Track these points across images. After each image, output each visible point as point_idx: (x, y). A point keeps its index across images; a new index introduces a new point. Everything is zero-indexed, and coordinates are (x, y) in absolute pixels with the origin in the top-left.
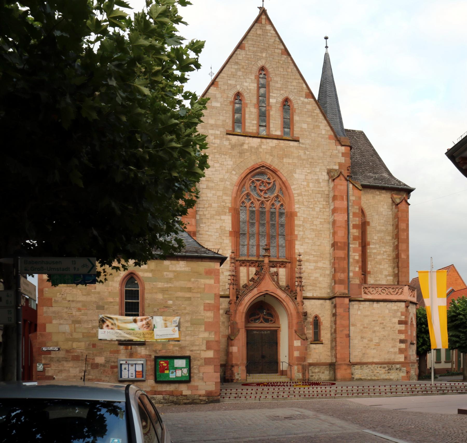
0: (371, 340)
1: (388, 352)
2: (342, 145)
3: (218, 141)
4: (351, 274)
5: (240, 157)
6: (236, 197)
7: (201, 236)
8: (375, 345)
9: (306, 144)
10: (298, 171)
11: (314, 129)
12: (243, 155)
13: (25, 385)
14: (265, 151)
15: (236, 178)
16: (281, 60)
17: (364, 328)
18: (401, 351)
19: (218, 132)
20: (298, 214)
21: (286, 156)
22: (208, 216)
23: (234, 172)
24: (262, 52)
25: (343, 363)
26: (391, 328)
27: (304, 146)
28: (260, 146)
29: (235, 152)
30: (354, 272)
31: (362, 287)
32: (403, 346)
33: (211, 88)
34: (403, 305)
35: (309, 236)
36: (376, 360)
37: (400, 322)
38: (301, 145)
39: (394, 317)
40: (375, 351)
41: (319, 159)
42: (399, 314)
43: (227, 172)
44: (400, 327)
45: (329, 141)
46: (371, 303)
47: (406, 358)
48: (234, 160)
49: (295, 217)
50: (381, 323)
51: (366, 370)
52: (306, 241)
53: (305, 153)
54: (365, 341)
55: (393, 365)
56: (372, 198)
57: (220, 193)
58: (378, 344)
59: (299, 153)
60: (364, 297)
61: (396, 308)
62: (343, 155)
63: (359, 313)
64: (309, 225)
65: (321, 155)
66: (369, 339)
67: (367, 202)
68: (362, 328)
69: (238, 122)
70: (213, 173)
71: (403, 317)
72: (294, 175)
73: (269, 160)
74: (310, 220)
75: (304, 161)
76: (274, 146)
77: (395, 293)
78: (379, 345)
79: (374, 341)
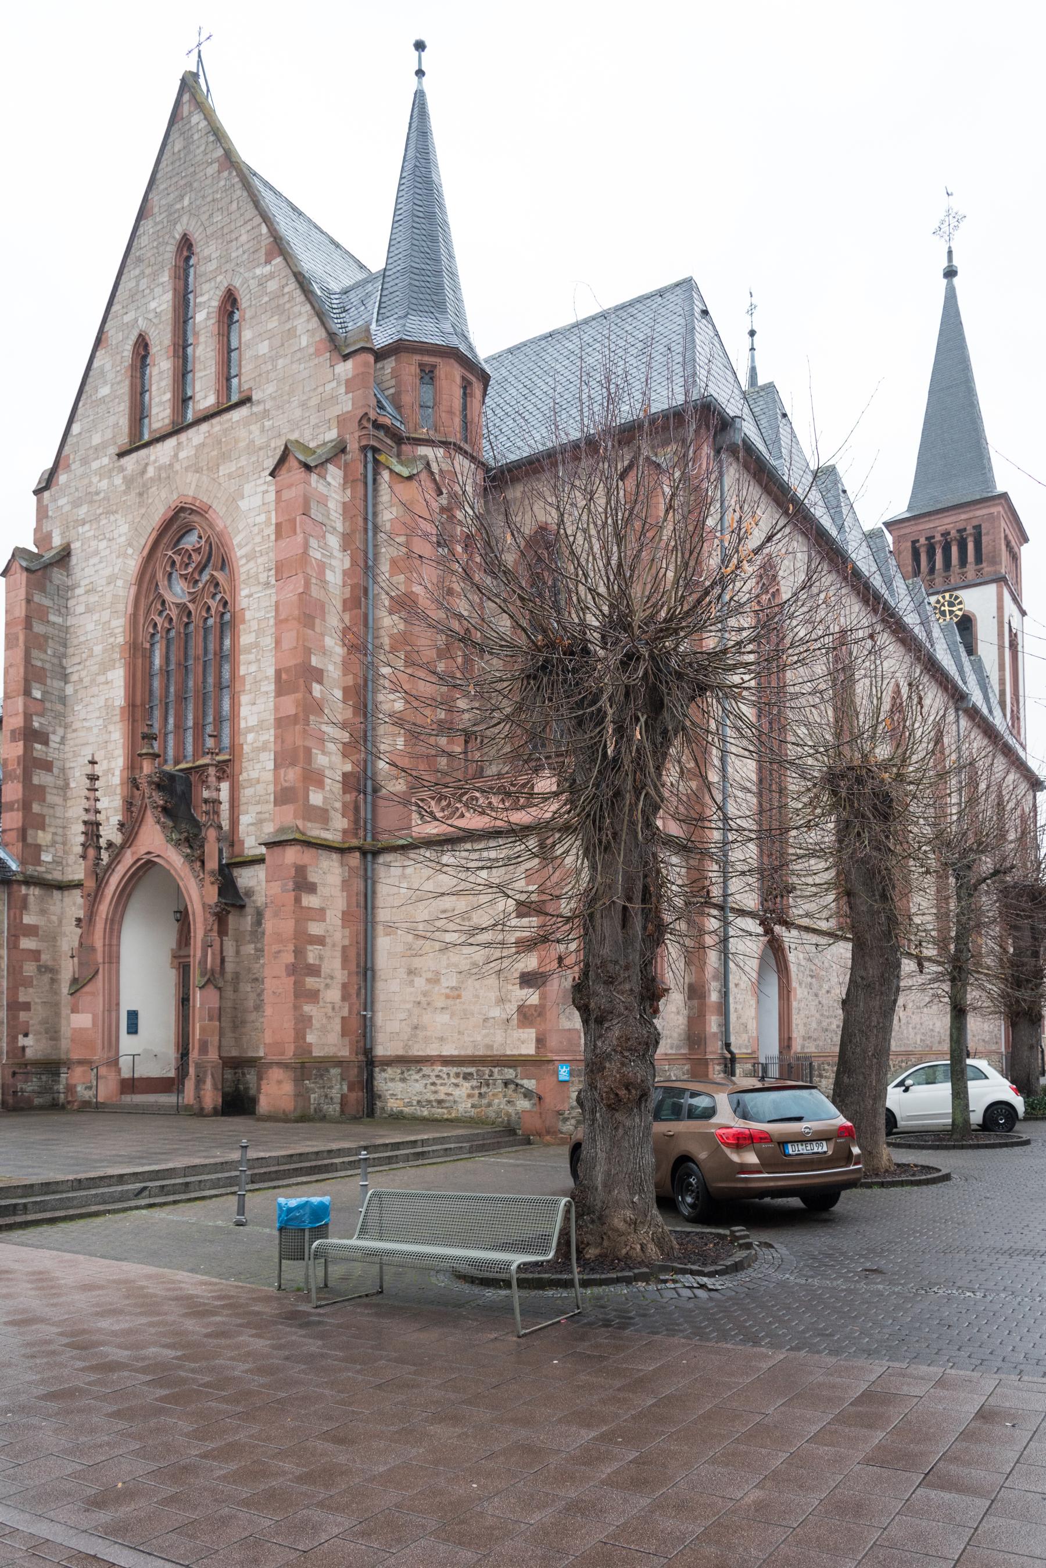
0: (435, 980)
1: (486, 1020)
2: (346, 357)
3: (104, 484)
5: (141, 505)
6: (135, 615)
7: (74, 735)
8: (448, 997)
9: (264, 401)
10: (248, 488)
11: (283, 345)
12: (145, 496)
13: (723, 1152)
15: (133, 564)
16: (217, 192)
18: (526, 1016)
19: (105, 461)
20: (248, 615)
21: (225, 457)
22: (87, 681)
23: (130, 551)
24: (182, 197)
28: (176, 455)
29: (132, 498)
32: (532, 997)
33: (98, 354)
36: (449, 1050)
40: (444, 1018)
41: (293, 431)
43: (118, 557)
45: (316, 361)
47: (540, 1041)
48: (130, 517)
49: (241, 627)
51: (417, 1085)
52: (263, 689)
53: (263, 430)
54: (420, 982)
55: (496, 1070)
58: (455, 994)
59: (250, 433)
65: (298, 413)
66: (430, 975)
69: (139, 413)
70: (96, 568)
72: (239, 503)
73: (189, 487)
75: (261, 453)
76: (202, 441)
78: (459, 997)
79: (445, 982)
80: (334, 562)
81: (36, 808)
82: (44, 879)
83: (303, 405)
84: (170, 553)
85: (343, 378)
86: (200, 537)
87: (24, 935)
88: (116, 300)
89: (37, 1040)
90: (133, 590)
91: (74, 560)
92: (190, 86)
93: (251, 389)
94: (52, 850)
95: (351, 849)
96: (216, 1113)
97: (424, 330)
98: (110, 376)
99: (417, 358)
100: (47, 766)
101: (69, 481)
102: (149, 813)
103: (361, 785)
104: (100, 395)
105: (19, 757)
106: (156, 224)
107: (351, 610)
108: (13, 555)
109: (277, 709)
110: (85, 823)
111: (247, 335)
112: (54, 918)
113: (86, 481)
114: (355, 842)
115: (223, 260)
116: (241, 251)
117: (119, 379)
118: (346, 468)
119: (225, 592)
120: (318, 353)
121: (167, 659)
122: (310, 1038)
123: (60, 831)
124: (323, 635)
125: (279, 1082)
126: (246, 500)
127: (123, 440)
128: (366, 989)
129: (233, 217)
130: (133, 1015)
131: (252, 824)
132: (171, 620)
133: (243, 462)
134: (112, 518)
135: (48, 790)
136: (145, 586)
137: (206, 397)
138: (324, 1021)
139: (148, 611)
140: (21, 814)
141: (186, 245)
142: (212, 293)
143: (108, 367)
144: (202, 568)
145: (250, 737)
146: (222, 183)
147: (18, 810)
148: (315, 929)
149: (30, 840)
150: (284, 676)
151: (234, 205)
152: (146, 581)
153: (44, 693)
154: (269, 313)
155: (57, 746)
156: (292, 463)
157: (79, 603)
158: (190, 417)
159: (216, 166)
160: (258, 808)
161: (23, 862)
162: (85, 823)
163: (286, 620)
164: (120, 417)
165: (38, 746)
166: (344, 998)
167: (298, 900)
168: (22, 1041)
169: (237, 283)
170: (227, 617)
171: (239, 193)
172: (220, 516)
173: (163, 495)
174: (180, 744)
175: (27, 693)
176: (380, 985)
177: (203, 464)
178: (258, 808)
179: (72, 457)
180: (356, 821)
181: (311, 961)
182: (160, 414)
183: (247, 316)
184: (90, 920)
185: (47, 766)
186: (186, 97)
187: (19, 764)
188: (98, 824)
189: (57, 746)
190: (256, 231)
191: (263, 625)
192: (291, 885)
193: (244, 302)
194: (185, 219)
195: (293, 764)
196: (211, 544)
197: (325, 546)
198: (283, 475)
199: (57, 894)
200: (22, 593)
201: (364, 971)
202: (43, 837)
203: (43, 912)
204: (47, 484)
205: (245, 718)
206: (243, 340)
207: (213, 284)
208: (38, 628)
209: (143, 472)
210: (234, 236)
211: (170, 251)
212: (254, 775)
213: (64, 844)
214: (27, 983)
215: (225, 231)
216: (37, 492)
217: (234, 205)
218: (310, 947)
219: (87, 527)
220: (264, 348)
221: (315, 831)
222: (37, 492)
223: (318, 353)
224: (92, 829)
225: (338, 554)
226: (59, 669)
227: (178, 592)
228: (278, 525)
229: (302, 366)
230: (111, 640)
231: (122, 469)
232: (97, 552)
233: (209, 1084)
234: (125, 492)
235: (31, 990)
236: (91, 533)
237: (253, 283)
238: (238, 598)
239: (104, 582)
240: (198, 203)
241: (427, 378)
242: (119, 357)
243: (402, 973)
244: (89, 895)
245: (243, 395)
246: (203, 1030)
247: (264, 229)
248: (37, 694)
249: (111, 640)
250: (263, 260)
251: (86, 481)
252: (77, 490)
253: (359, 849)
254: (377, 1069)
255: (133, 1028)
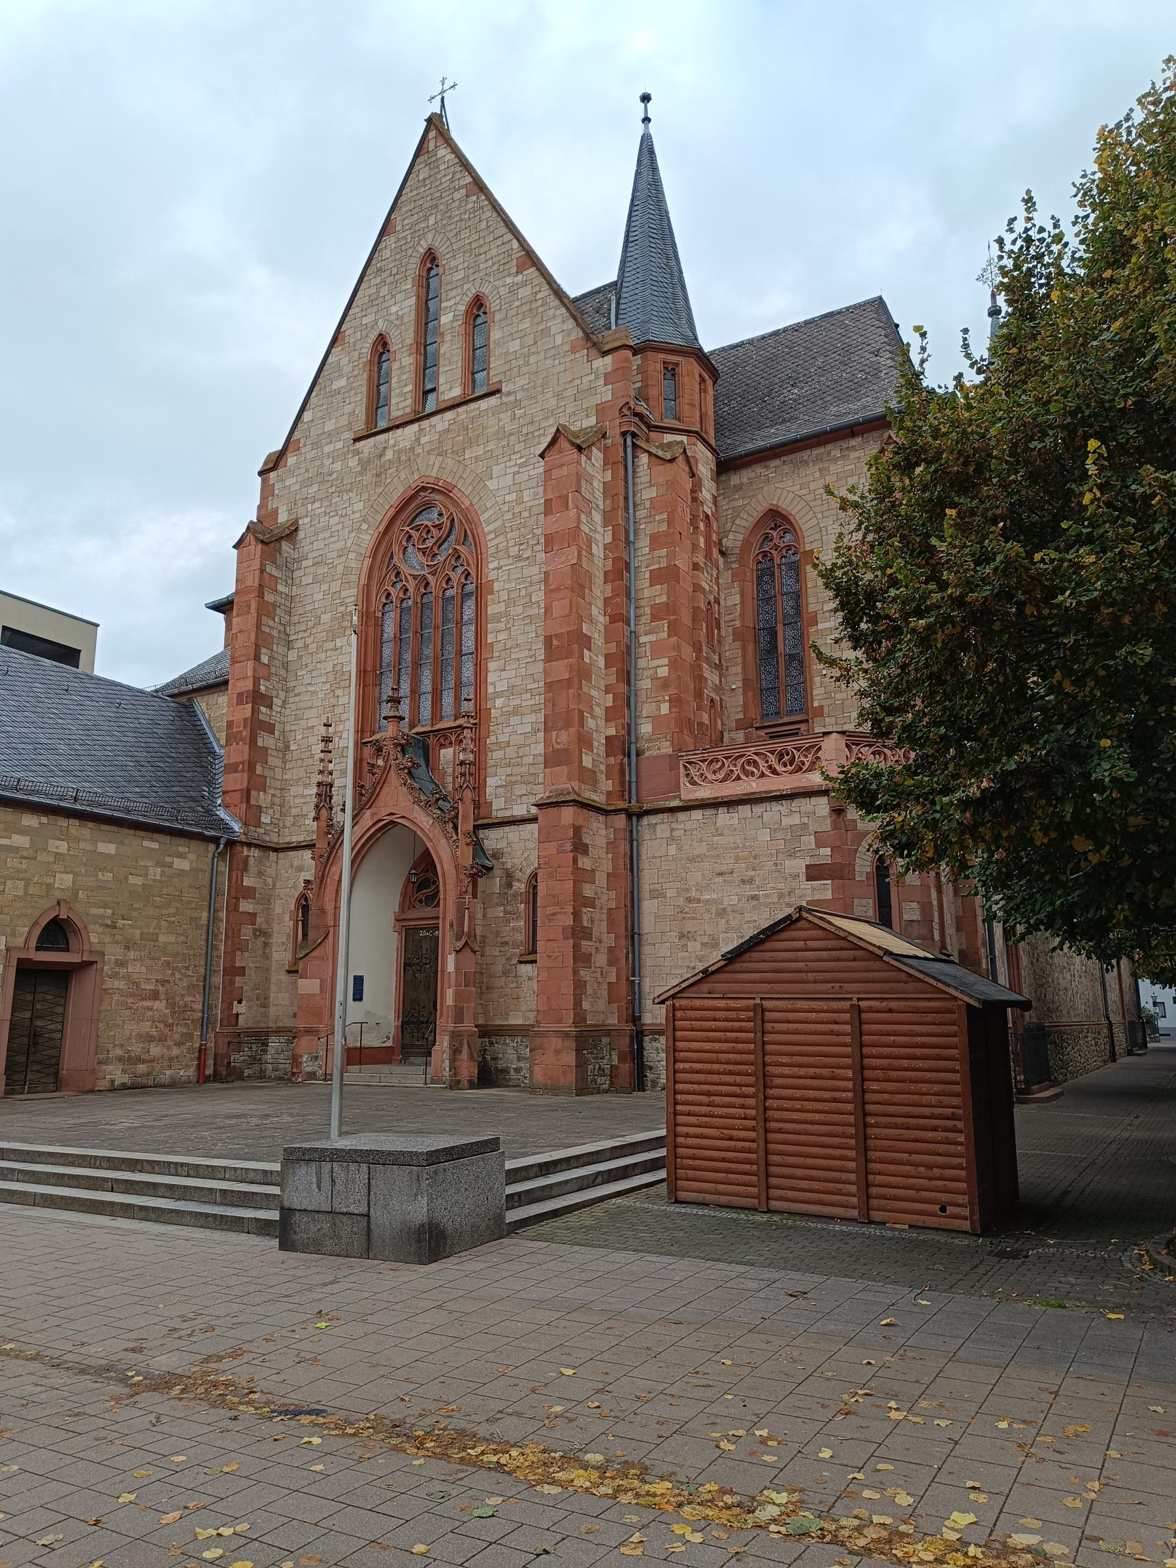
2: (605, 353)
4: (646, 728)
6: (368, 585)
11: (535, 343)
14: (419, 452)
15: (368, 539)
17: (689, 900)
20: (497, 586)
21: (471, 442)
22: (312, 648)
24: (426, 218)
25: (553, 1027)
26: (781, 896)
27: (512, 398)
28: (418, 440)
29: (369, 477)
30: (655, 720)
31: (681, 763)
34: (822, 806)
35: (521, 639)
37: (814, 873)
38: (505, 399)
39: (792, 855)
42: (809, 841)
44: (813, 889)
46: (709, 812)
50: (743, 881)
53: (514, 418)
56: (817, 475)
57: (335, 586)
59: (500, 420)
60: (689, 793)
61: (796, 820)
62: (608, 378)
63: (672, 850)
64: (520, 609)
65: (553, 402)
66: (705, 939)
67: (805, 492)
68: (681, 901)
71: (827, 851)
73: (432, 469)
74: (523, 593)
75: (512, 438)
77: (720, 776)
80: (599, 537)
81: (259, 770)
82: (264, 841)
83: (559, 395)
84: (407, 529)
85: (602, 371)
86: (441, 515)
87: (244, 898)
88: (354, 304)
89: (250, 1007)
90: (367, 562)
91: (301, 534)
92: (436, 125)
93: (500, 382)
94: (271, 811)
95: (616, 812)
96: (472, 1086)
97: (661, 332)
98: (346, 370)
99: (662, 356)
100: (270, 729)
101: (298, 463)
102: (393, 774)
103: (624, 747)
104: (334, 387)
105: (245, 720)
106: (399, 240)
107: (613, 581)
108: (248, 528)
109: (546, 672)
110: (319, 784)
111: (496, 334)
112: (270, 880)
113: (318, 463)
114: (621, 805)
115: (471, 271)
116: (490, 263)
117: (356, 372)
118: (605, 450)
119: (468, 564)
120: (574, 350)
121: (401, 629)
122: (586, 1005)
123: (278, 793)
124: (590, 604)
125: (558, 1052)
126: (495, 481)
127: (360, 426)
128: (634, 953)
129: (482, 234)
130: (359, 981)
131: (501, 786)
132: (407, 590)
133: (491, 446)
134: (345, 496)
135: (270, 752)
136: (379, 559)
137: (451, 388)
138: (595, 987)
139: (382, 582)
140: (246, 775)
141: (431, 257)
142: (458, 299)
143: (344, 361)
144: (440, 543)
145: (499, 702)
146: (471, 205)
147: (243, 771)
148: (588, 891)
149: (253, 802)
150: (555, 642)
151: (484, 225)
152: (382, 554)
153: (271, 658)
154: (520, 317)
155: (279, 709)
156: (563, 443)
157: (305, 574)
158: (431, 406)
159: (463, 191)
160: (509, 771)
161: (246, 824)
162: (319, 784)
163: (558, 589)
164: (358, 405)
165: (263, 709)
166: (610, 963)
167: (575, 861)
168: (237, 1008)
169: (486, 290)
170: (471, 588)
171: (488, 214)
172: (465, 490)
173: (403, 476)
174: (415, 708)
175: (257, 658)
176: (647, 950)
177: (447, 447)
178: (509, 771)
179: (302, 441)
180: (622, 784)
181: (585, 924)
182: (401, 401)
183: (496, 319)
184: (322, 881)
185: (270, 729)
186: (432, 134)
187: (245, 727)
188: (331, 786)
189: (279, 709)
190: (507, 247)
191: (514, 595)
192: (568, 846)
193: (493, 304)
194: (430, 236)
195: (566, 726)
196: (453, 520)
197: (591, 521)
198: (552, 457)
199: (272, 855)
200: (256, 564)
201: (633, 936)
202: (263, 799)
203: (260, 874)
204: (274, 463)
205: (494, 684)
206: (492, 339)
207: (459, 291)
208: (269, 597)
209: (381, 455)
210: (482, 250)
211: (413, 265)
212: (503, 738)
213: (281, 806)
214: (242, 947)
215: (473, 246)
216: (261, 473)
217: (484, 225)
218: (584, 910)
219: (317, 504)
220: (515, 346)
221: (590, 795)
222: (261, 473)
223: (574, 350)
224: (325, 792)
225: (600, 529)
226: (282, 636)
227: (413, 563)
228: (548, 503)
229: (557, 362)
230: (342, 609)
231: (357, 452)
232: (328, 527)
233: (465, 1054)
234: (360, 473)
235: (246, 954)
236: (323, 510)
237: (503, 291)
238: (485, 570)
239: (335, 554)
240: (445, 222)
241: (669, 375)
242: (356, 353)
243: (673, 936)
244: (321, 856)
245: (493, 388)
246: (458, 996)
247: (515, 244)
248: (265, 659)
249: (342, 609)
250: (514, 270)
251: (318, 463)
252: (307, 471)
253: (626, 810)
254: (647, 1039)
255: (358, 996)
